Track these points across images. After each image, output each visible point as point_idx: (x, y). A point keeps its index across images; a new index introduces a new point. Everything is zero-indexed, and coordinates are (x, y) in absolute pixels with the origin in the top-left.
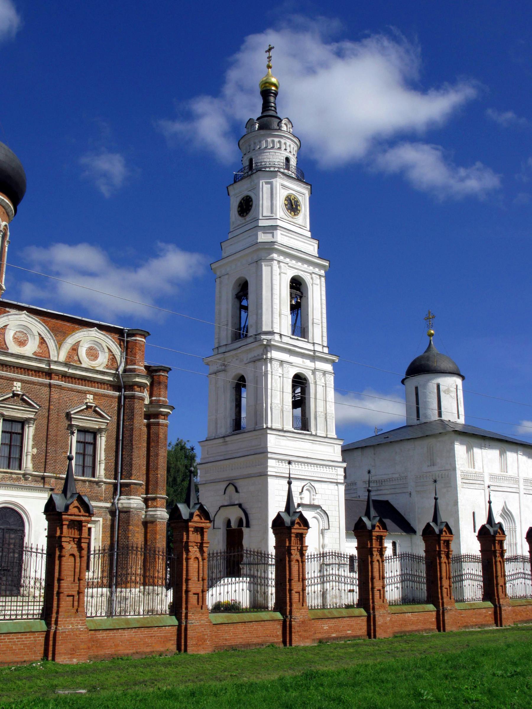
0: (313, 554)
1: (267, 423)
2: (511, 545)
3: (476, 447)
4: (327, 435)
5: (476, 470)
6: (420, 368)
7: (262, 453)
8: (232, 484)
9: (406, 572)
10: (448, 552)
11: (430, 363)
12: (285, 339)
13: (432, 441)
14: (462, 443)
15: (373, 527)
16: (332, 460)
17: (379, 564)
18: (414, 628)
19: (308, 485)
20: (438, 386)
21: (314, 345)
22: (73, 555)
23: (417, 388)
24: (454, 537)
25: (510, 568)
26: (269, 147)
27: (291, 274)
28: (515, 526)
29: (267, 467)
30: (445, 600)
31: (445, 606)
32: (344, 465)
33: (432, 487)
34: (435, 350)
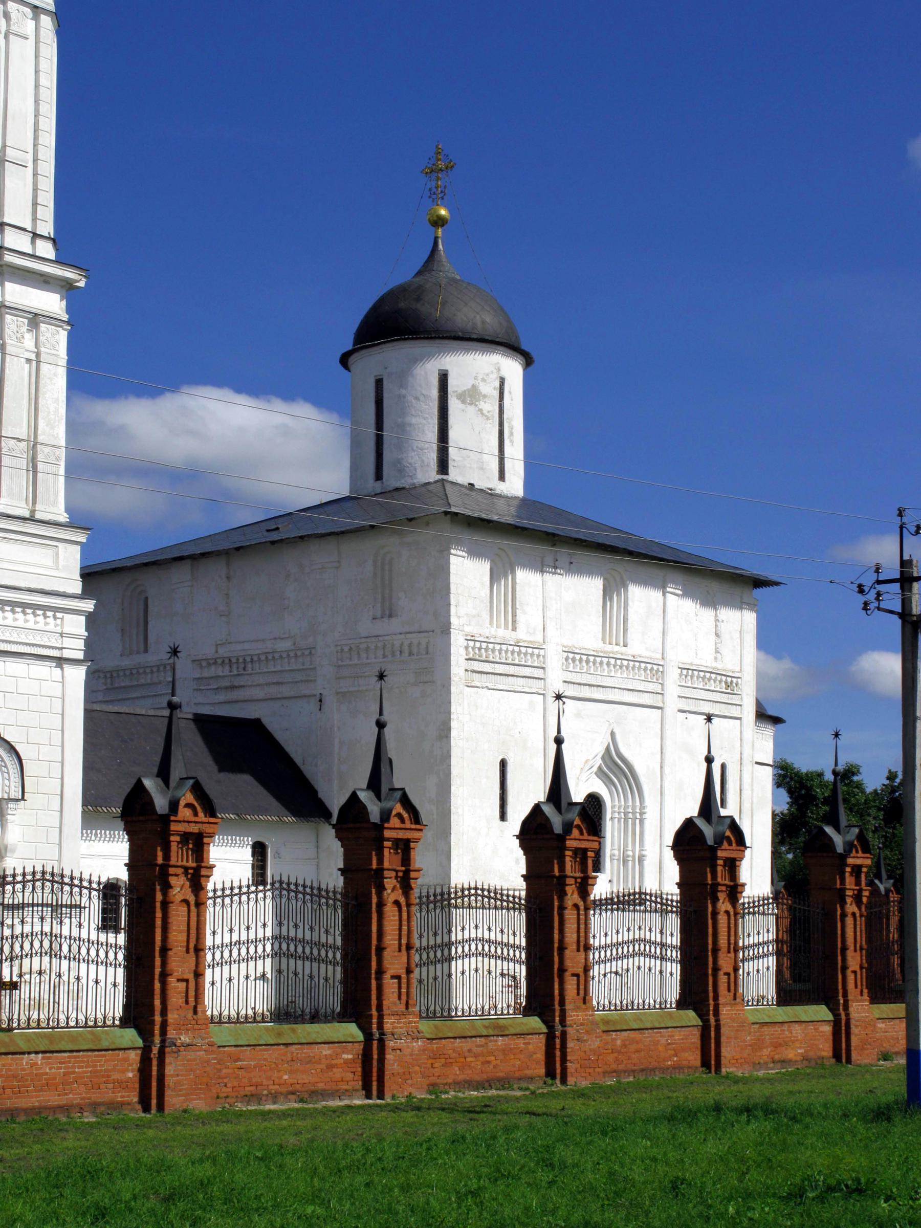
0: (236, 884)
2: (625, 862)
3: (524, 566)
4: (33, 512)
5: (522, 634)
6: (398, 322)
9: (37, 928)
10: (407, 872)
11: (424, 308)
13: (389, 543)
14: (474, 553)
15: (386, 815)
16: (47, 588)
17: (400, 911)
18: (53, 1099)
20: (443, 378)
22: (186, 902)
23: (379, 383)
24: (427, 835)
25: (604, 928)
28: (642, 807)
30: (172, 1017)
31: (171, 1033)
32: (89, 605)
33: (831, 740)
34: (448, 268)
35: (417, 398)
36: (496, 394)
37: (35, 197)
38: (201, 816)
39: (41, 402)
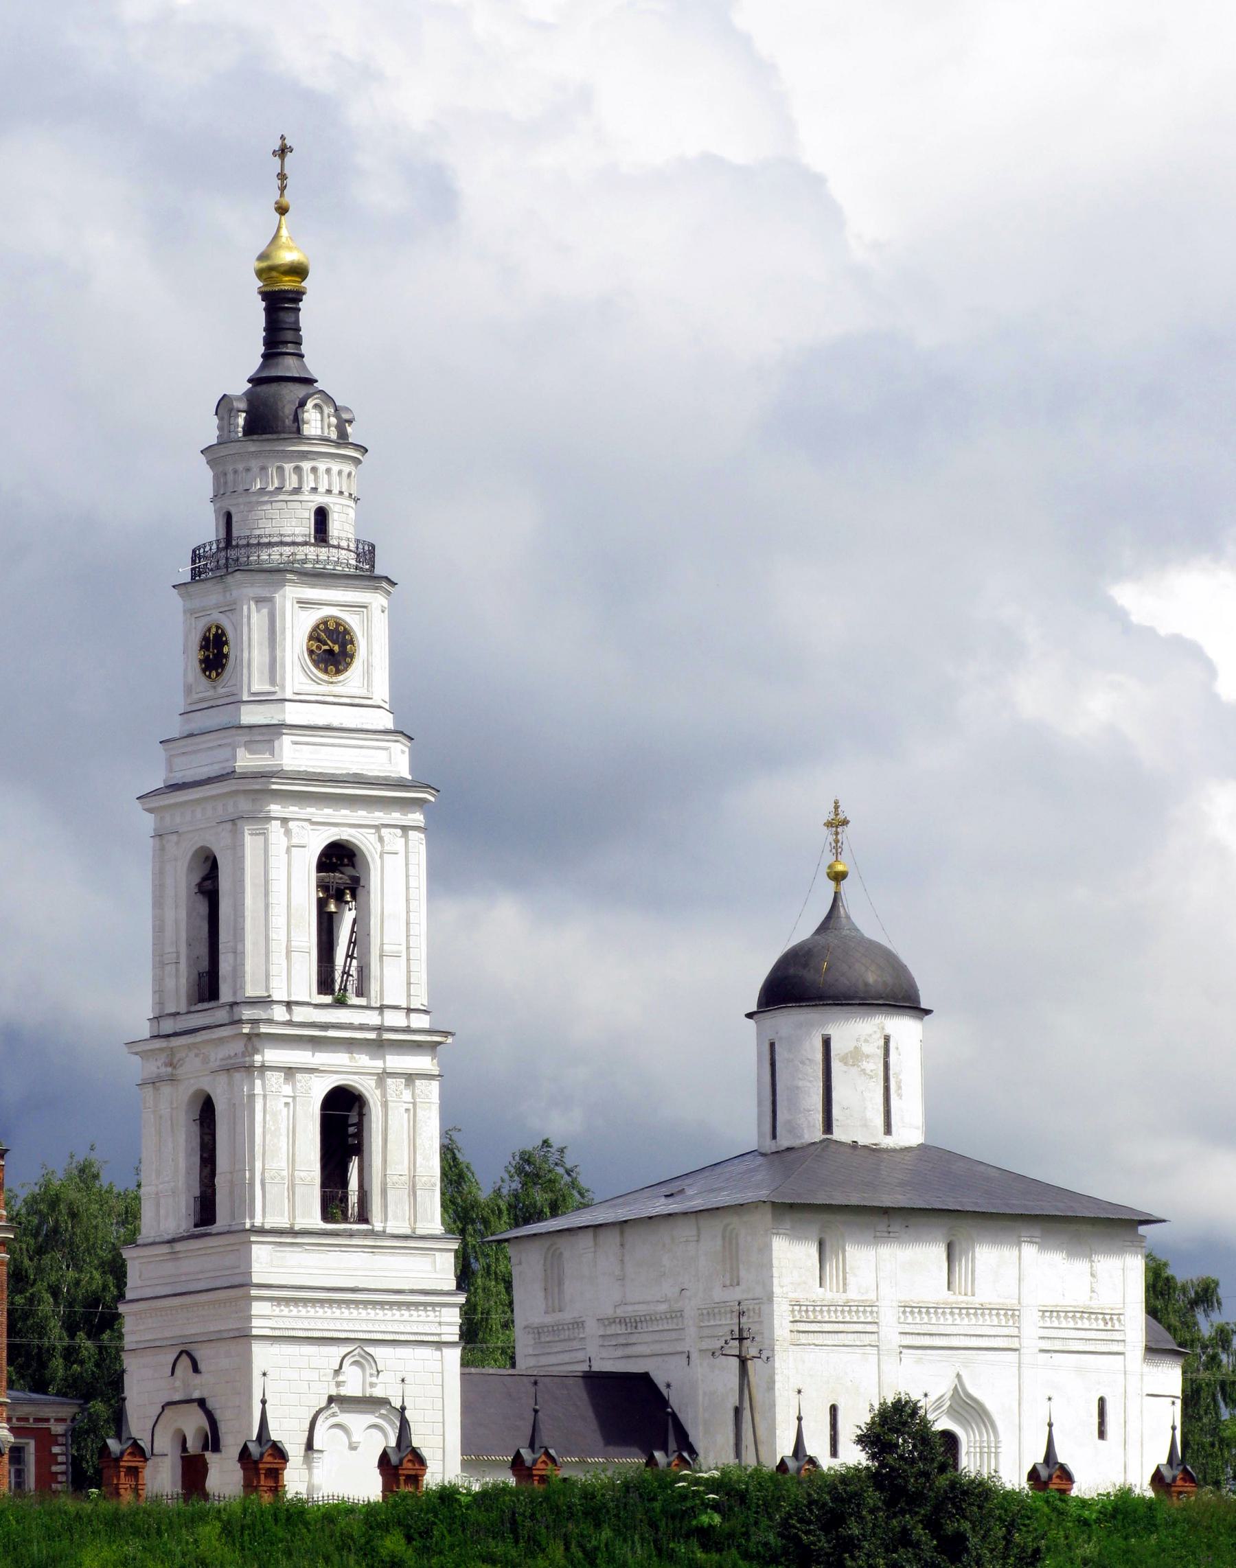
1: (252, 1217)
7: (240, 1287)
8: (188, 1358)
11: (809, 975)
12: (300, 1014)
14: (796, 1236)
19: (356, 1352)
20: (827, 1043)
21: (381, 1014)
26: (271, 488)
27: (318, 841)
28: (997, 1441)
29: (249, 1318)
32: (461, 1299)
35: (803, 1063)
36: (881, 1052)
37: (409, 978)
38: (417, 1467)
39: (418, 1142)
